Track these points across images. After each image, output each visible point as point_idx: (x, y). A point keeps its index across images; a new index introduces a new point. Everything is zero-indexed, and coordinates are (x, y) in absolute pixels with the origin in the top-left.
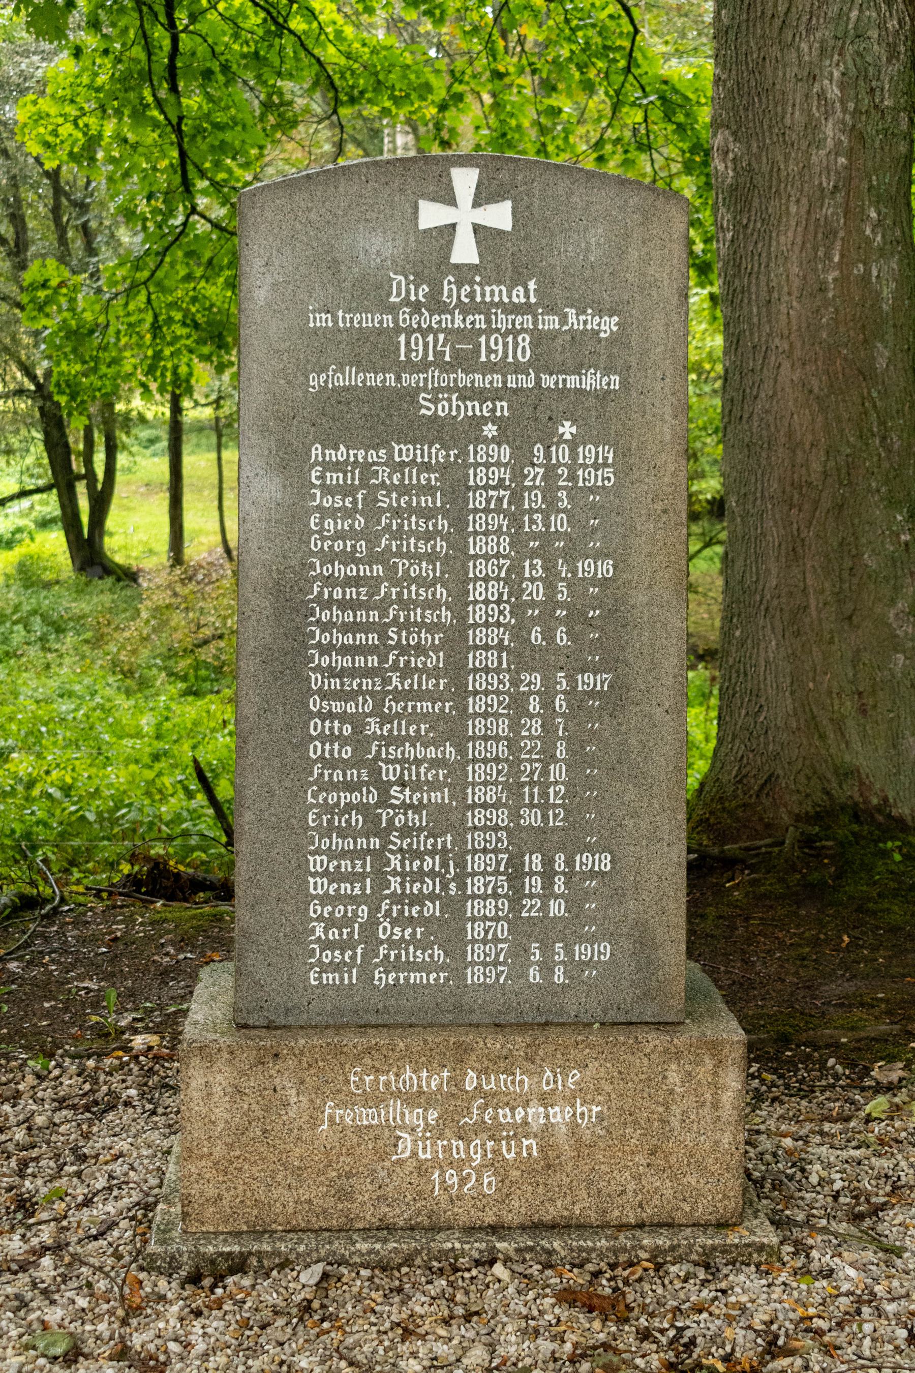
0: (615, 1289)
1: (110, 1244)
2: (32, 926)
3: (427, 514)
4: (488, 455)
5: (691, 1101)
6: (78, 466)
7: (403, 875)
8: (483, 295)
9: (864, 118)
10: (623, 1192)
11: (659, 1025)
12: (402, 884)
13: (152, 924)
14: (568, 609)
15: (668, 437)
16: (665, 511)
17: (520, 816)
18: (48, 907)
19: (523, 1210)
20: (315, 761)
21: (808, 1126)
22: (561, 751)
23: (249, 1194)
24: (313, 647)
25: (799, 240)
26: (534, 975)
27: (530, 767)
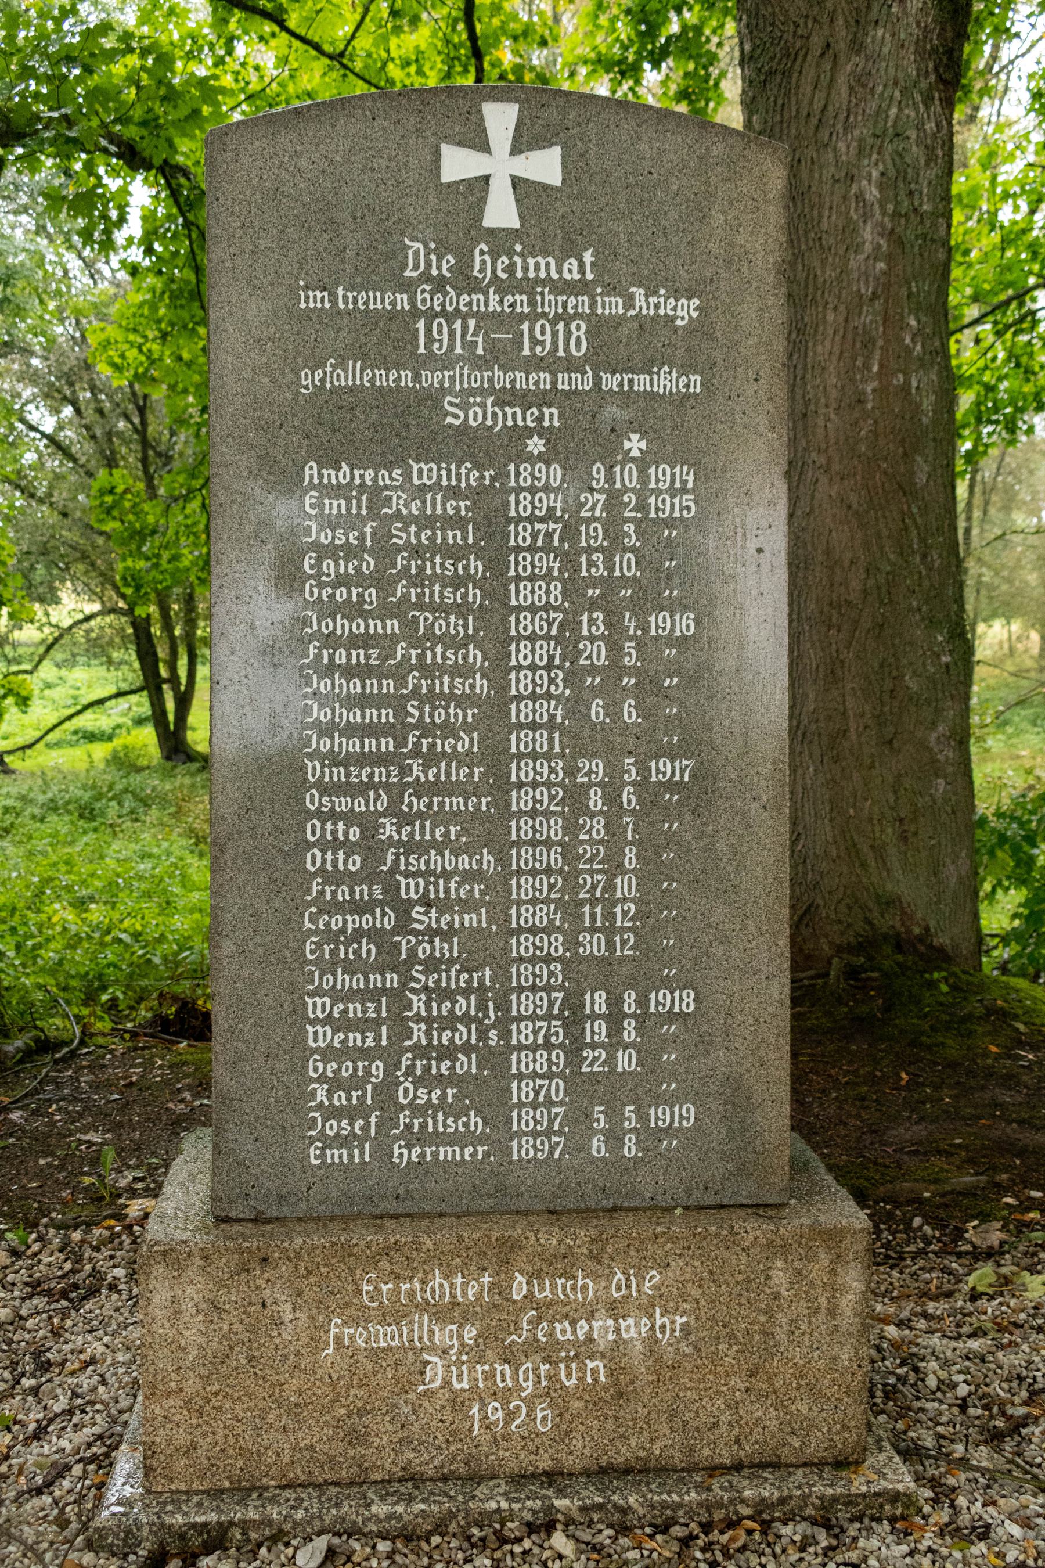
1: (56, 1502)
3: (456, 553)
4: (534, 477)
6: (164, 672)
7: (429, 1020)
8: (525, 269)
9: (903, 221)
10: (716, 1425)
11: (758, 1208)
12: (428, 1033)
13: (170, 1067)
17: (579, 944)
18: (65, 1050)
20: (314, 875)
22: (630, 858)
23: (231, 1440)
25: (836, 350)
26: (598, 1147)
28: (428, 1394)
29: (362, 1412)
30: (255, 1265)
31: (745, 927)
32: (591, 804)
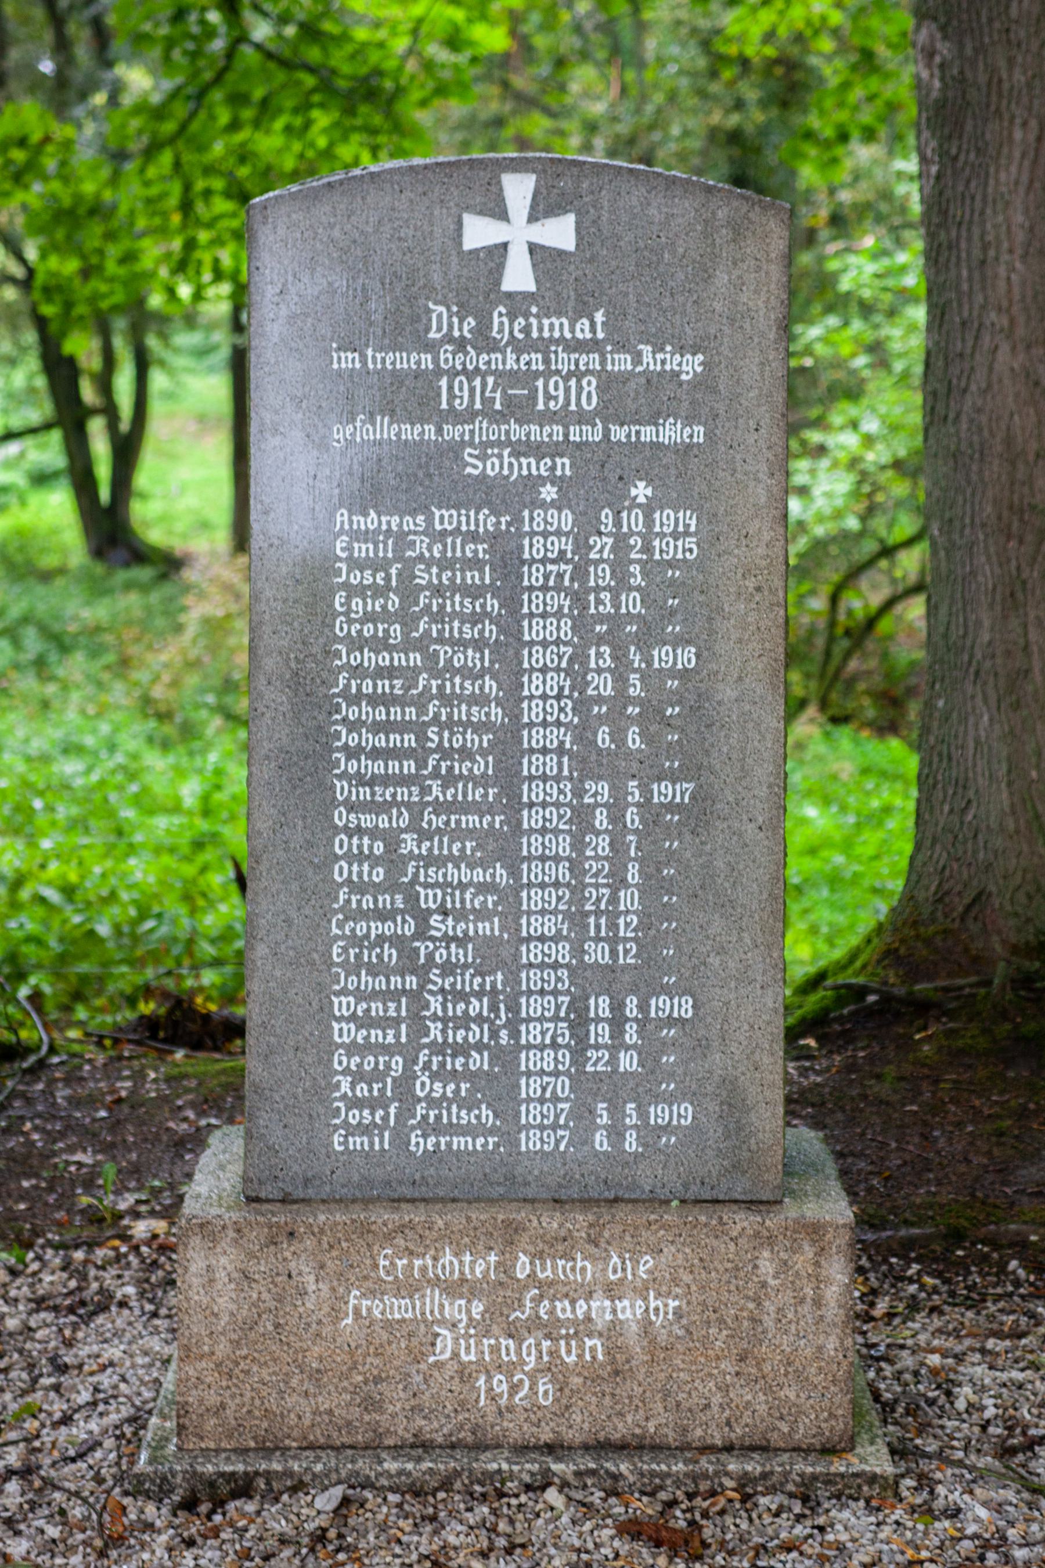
0: (692, 1523)
2: (10, 1084)
3: (474, 592)
4: (546, 522)
5: (787, 1297)
6: (88, 393)
7: (445, 1020)
8: (541, 329)
10: (707, 1406)
11: (752, 1204)
12: (444, 1031)
14: (641, 706)
15: (763, 500)
16: (758, 589)
17: (584, 952)
18: (32, 1059)
19: (586, 1426)
20: (341, 885)
21: (968, 1342)
22: (633, 874)
23: (257, 1402)
24: (338, 750)
25: (1025, 178)
26: (601, 1141)
27: (596, 894)
28: (439, 1365)
29: (377, 1380)
30: (282, 1238)
31: (740, 939)
32: (597, 823)
